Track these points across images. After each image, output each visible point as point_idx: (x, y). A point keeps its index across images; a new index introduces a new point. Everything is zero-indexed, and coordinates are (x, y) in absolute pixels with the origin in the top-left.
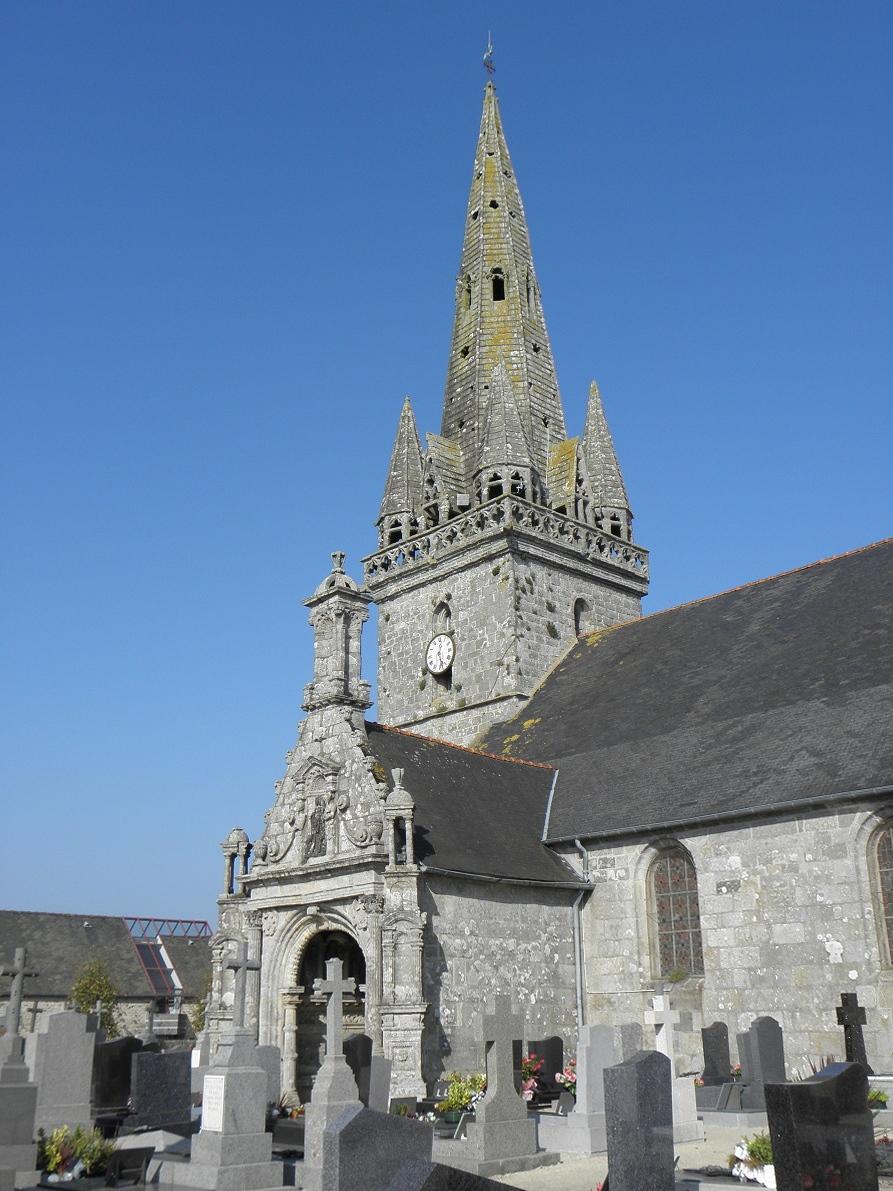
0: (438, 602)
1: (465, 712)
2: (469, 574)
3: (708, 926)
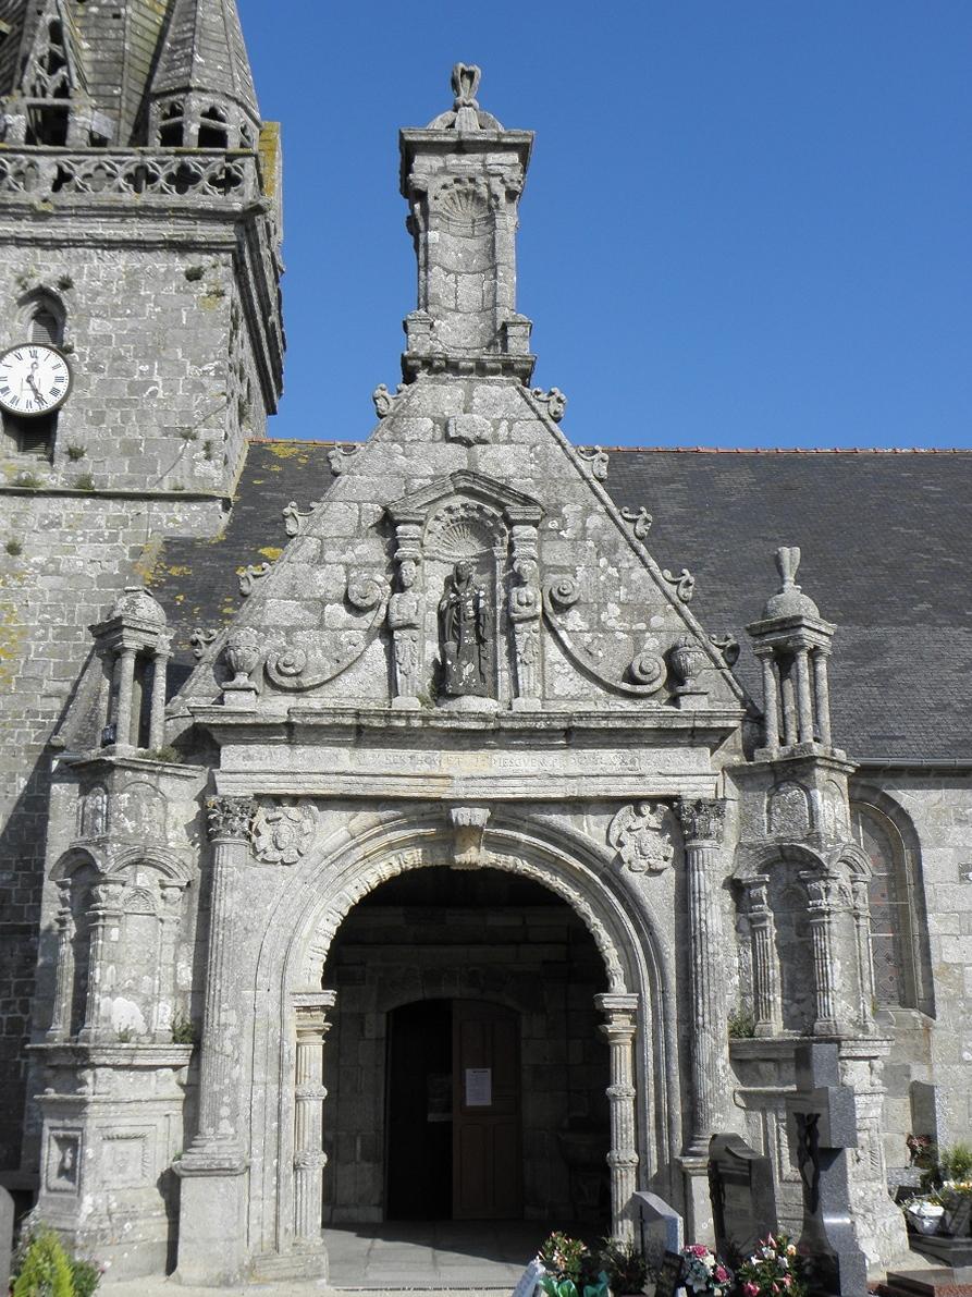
0: (34, 284)
1: (87, 502)
2: (123, 260)
3: (942, 930)
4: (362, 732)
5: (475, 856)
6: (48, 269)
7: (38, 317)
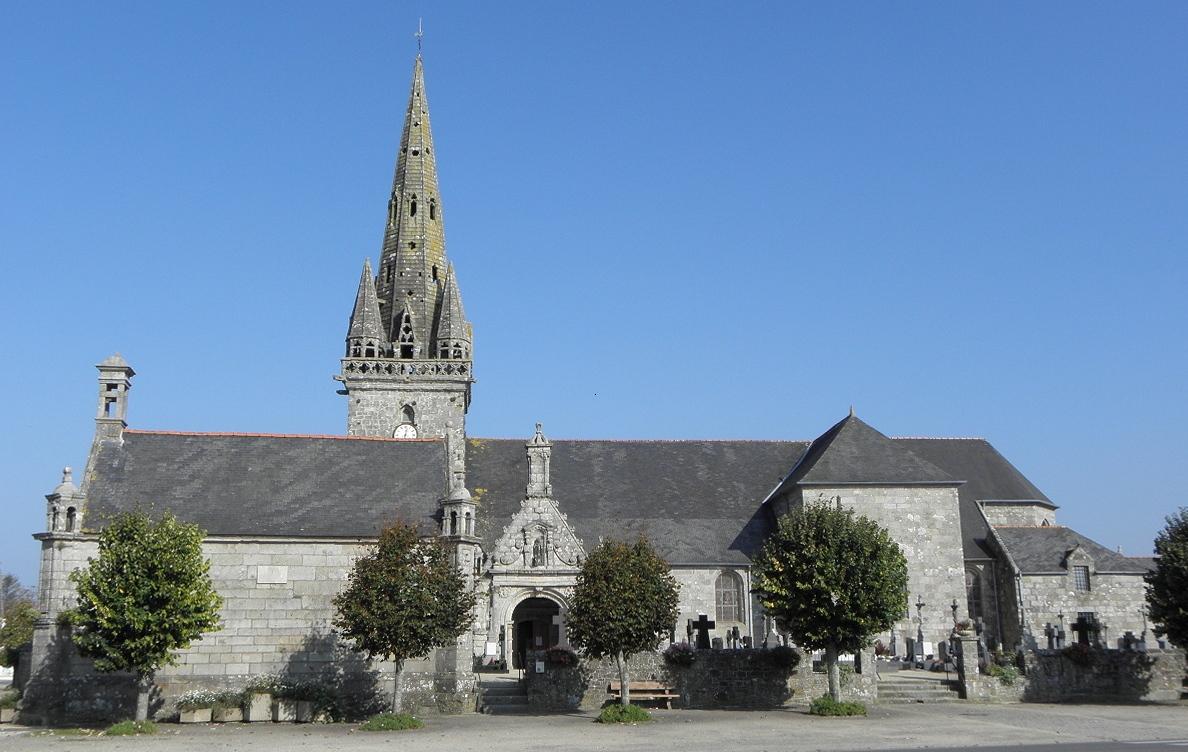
5: (539, 596)
6: (409, 399)
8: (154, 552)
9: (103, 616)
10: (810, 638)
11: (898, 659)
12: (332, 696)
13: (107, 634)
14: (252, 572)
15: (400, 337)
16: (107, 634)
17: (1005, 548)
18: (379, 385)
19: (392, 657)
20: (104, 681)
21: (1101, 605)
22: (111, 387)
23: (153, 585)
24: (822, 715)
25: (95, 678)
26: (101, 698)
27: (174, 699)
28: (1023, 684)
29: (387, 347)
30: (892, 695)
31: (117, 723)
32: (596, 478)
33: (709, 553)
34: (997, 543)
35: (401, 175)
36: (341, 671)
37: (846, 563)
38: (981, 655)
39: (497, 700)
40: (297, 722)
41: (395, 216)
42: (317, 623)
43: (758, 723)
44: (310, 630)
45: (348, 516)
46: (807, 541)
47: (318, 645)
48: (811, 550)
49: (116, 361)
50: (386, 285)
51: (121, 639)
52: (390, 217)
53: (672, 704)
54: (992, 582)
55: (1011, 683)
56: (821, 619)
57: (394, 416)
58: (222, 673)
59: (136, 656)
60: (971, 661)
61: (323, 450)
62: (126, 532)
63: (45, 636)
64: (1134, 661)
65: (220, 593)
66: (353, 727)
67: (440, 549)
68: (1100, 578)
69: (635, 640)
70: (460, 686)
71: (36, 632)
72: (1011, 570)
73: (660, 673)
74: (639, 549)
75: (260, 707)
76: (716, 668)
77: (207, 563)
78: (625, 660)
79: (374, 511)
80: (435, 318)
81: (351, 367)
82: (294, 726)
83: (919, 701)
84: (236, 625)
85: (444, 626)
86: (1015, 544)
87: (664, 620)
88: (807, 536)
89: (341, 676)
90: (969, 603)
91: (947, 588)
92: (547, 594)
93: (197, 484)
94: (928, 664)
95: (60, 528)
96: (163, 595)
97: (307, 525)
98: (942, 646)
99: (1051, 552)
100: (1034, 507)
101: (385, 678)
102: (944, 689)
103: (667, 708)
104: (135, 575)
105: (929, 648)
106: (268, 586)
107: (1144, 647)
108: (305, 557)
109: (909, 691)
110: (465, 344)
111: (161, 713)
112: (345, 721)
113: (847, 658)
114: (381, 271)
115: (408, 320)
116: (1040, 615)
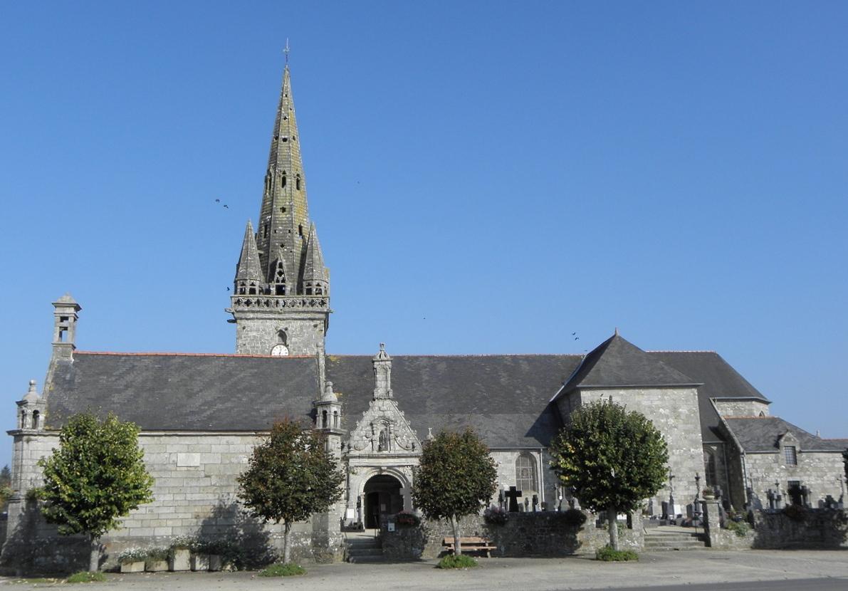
0: (279, 329)
4: (369, 457)
5: (384, 473)
6: (282, 325)
7: (279, 335)
8: (102, 444)
9: (64, 493)
10: (596, 503)
11: (655, 517)
12: (236, 551)
13: (67, 506)
14: (174, 458)
15: (275, 279)
16: (67, 506)
17: (732, 434)
18: (260, 315)
19: (282, 521)
20: (64, 542)
21: (805, 475)
22: (63, 319)
23: (102, 468)
24: (605, 560)
25: (56, 540)
26: (60, 554)
27: (116, 555)
28: (752, 535)
29: (265, 286)
30: (655, 545)
31: (75, 573)
32: (424, 384)
33: (511, 440)
34: (726, 430)
35: (274, 157)
36: (241, 532)
37: (622, 445)
38: (721, 514)
39: (360, 552)
40: (210, 570)
41: (270, 187)
42: (223, 496)
43: (559, 567)
44: (217, 501)
45: (245, 415)
46: (593, 430)
47: (224, 512)
48: (596, 437)
49: (67, 300)
50: (263, 240)
51: (78, 510)
52: (266, 188)
53: (491, 554)
54: (723, 458)
55: (743, 535)
56: (604, 488)
57: (271, 339)
58: (151, 534)
59: (89, 522)
60: (714, 519)
61: (224, 365)
62: (80, 428)
63: (17, 508)
64: (835, 517)
65: (152, 474)
66: (254, 574)
67: (317, 439)
68: (804, 455)
69: (464, 507)
70: (331, 543)
71: (10, 505)
72: (737, 450)
73: (481, 531)
74: (467, 437)
75: (181, 561)
76: (523, 526)
77: (142, 451)
78: (457, 521)
79: (264, 411)
80: (300, 264)
81: (238, 302)
82: (208, 574)
83: (675, 549)
84: (162, 498)
85: (321, 497)
86: (741, 430)
87: (485, 491)
88: (593, 426)
89: (241, 536)
90: (706, 475)
91: (690, 464)
92: (389, 472)
93: (130, 392)
94: (679, 521)
95: (28, 426)
96: (110, 477)
97: (214, 422)
98: (689, 507)
99: (767, 436)
100: (754, 402)
101: (275, 537)
102: (694, 540)
103: (487, 557)
104: (89, 461)
105: (678, 509)
106: (186, 468)
107: (842, 506)
108: (213, 446)
109: (668, 542)
110: (324, 284)
111: (106, 565)
112: (246, 570)
113: (622, 517)
114: (260, 229)
115: (281, 266)
116: (760, 483)
